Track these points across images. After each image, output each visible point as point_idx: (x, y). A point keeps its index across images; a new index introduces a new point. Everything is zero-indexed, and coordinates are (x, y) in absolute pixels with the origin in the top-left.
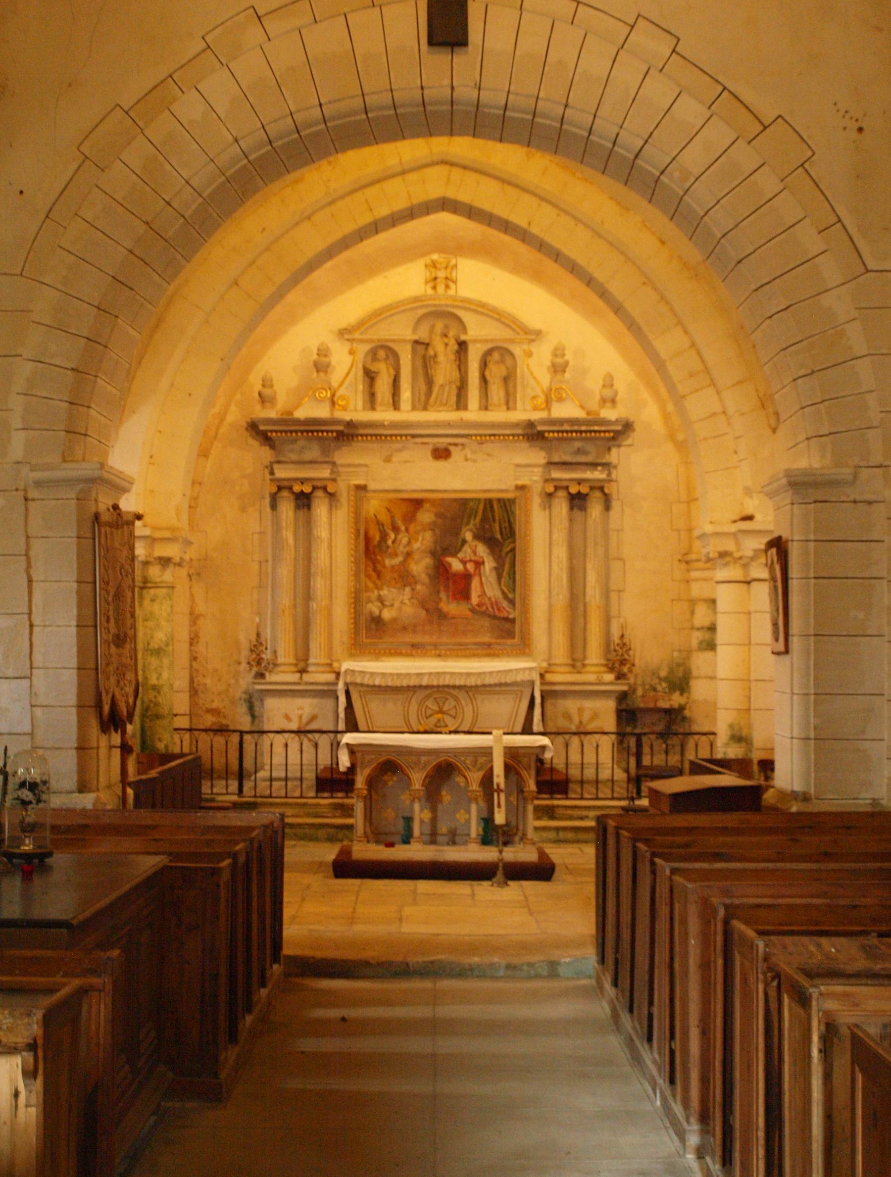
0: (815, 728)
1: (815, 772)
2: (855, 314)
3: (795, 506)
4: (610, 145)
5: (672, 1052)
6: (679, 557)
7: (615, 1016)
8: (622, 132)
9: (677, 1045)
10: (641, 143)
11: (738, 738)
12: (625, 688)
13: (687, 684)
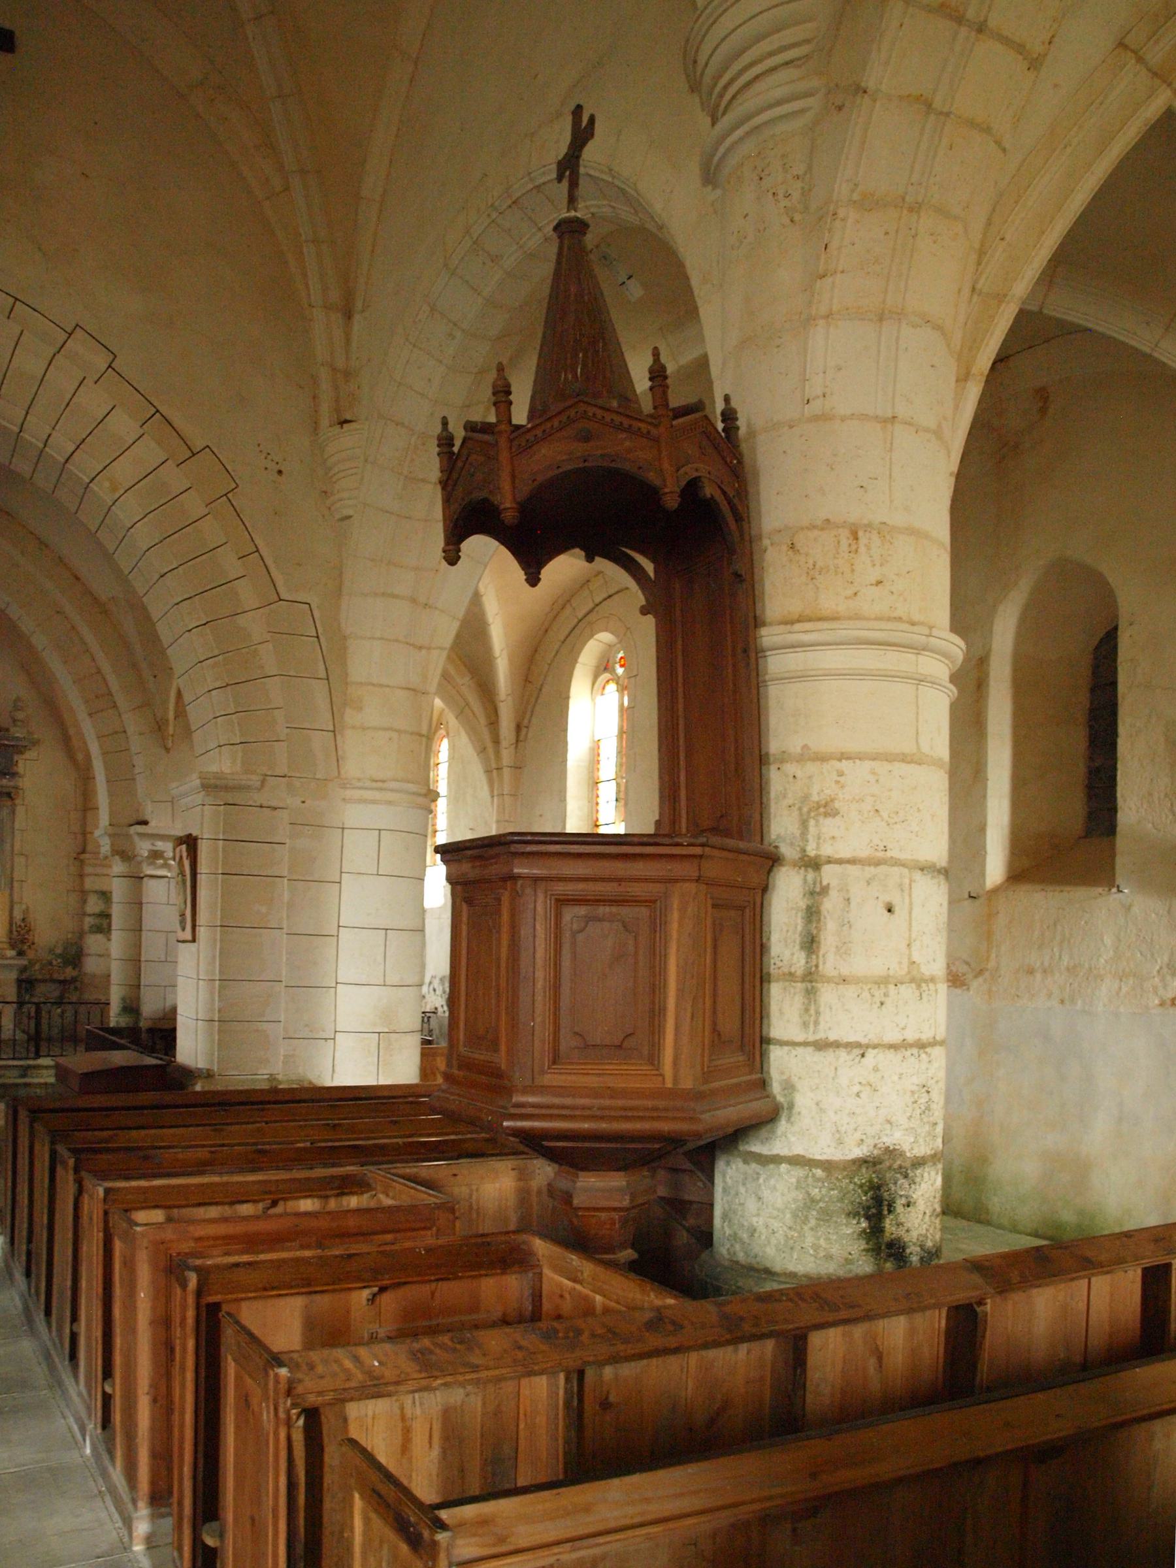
0: (219, 1011)
1: (218, 1051)
2: (268, 637)
3: (206, 807)
4: (41, 445)
5: (107, 1399)
6: (75, 855)
7: (27, 1312)
8: (54, 434)
9: (116, 1388)
10: (73, 447)
11: (131, 1008)
12: (26, 962)
13: (79, 959)
